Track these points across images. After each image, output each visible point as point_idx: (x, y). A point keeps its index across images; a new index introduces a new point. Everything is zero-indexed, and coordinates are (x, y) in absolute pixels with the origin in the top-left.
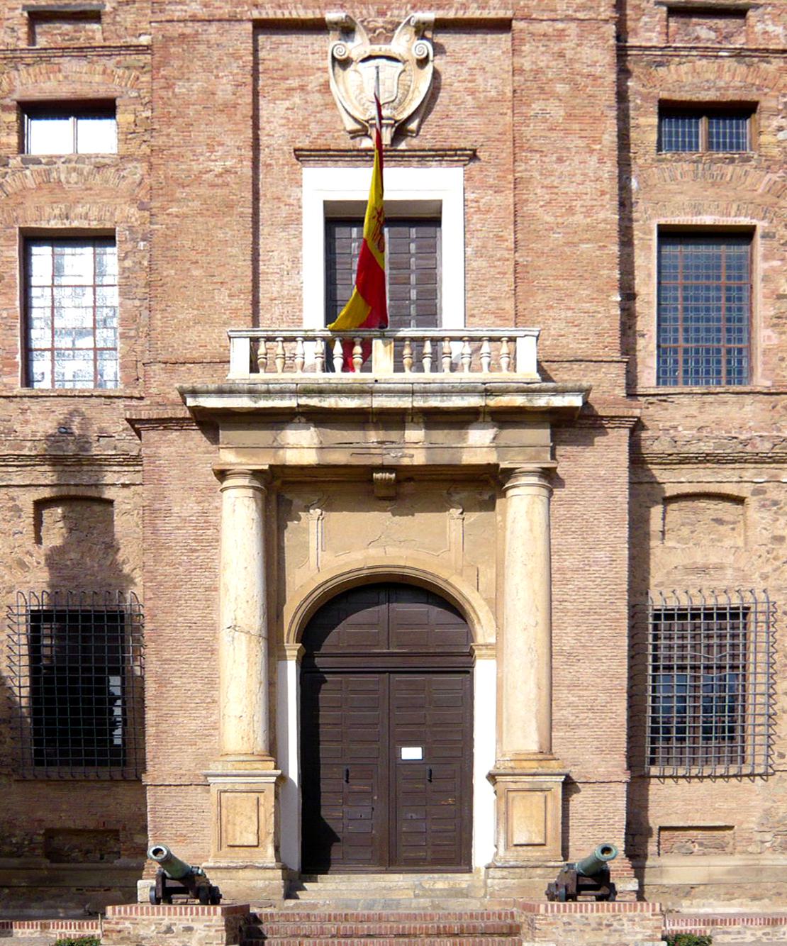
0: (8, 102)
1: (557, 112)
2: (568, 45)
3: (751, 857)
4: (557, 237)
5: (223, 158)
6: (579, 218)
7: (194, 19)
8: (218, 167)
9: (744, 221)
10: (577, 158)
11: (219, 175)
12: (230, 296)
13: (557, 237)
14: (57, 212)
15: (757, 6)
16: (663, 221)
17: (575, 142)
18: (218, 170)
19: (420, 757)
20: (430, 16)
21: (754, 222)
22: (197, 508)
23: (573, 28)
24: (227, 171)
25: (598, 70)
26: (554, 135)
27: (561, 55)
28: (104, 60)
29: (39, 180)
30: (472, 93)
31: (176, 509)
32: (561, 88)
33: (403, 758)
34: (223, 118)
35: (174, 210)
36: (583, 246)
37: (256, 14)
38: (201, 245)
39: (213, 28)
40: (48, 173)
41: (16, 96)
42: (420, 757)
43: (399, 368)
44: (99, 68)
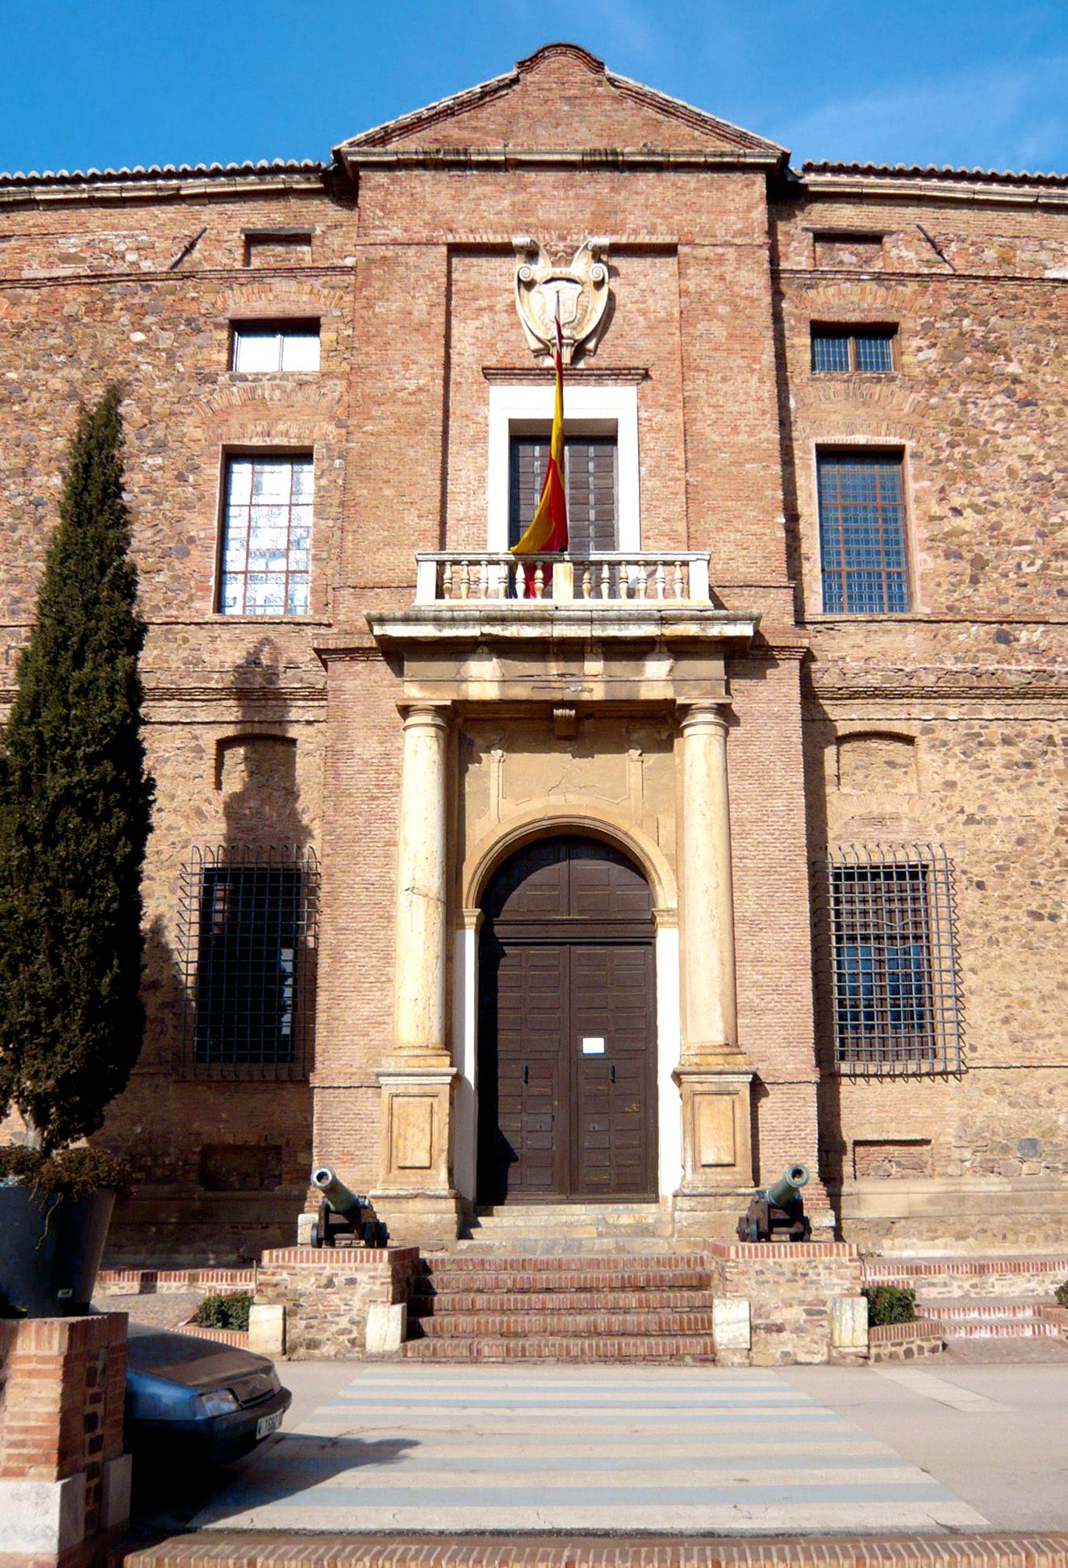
0: (221, 320)
1: (720, 332)
2: (728, 269)
6: (743, 438)
8: (412, 385)
9: (894, 440)
10: (739, 378)
11: (413, 393)
14: (259, 429)
15: (891, 233)
16: (820, 441)
18: (412, 388)
19: (602, 1050)
20: (605, 241)
21: (903, 441)
22: (380, 749)
23: (731, 253)
24: (420, 389)
26: (718, 355)
27: (722, 278)
28: (311, 281)
30: (644, 313)
31: (358, 751)
32: (722, 310)
35: (369, 428)
37: (450, 238)
38: (393, 464)
39: (412, 251)
41: (229, 315)
42: (602, 1050)
43: (578, 594)
44: (307, 288)
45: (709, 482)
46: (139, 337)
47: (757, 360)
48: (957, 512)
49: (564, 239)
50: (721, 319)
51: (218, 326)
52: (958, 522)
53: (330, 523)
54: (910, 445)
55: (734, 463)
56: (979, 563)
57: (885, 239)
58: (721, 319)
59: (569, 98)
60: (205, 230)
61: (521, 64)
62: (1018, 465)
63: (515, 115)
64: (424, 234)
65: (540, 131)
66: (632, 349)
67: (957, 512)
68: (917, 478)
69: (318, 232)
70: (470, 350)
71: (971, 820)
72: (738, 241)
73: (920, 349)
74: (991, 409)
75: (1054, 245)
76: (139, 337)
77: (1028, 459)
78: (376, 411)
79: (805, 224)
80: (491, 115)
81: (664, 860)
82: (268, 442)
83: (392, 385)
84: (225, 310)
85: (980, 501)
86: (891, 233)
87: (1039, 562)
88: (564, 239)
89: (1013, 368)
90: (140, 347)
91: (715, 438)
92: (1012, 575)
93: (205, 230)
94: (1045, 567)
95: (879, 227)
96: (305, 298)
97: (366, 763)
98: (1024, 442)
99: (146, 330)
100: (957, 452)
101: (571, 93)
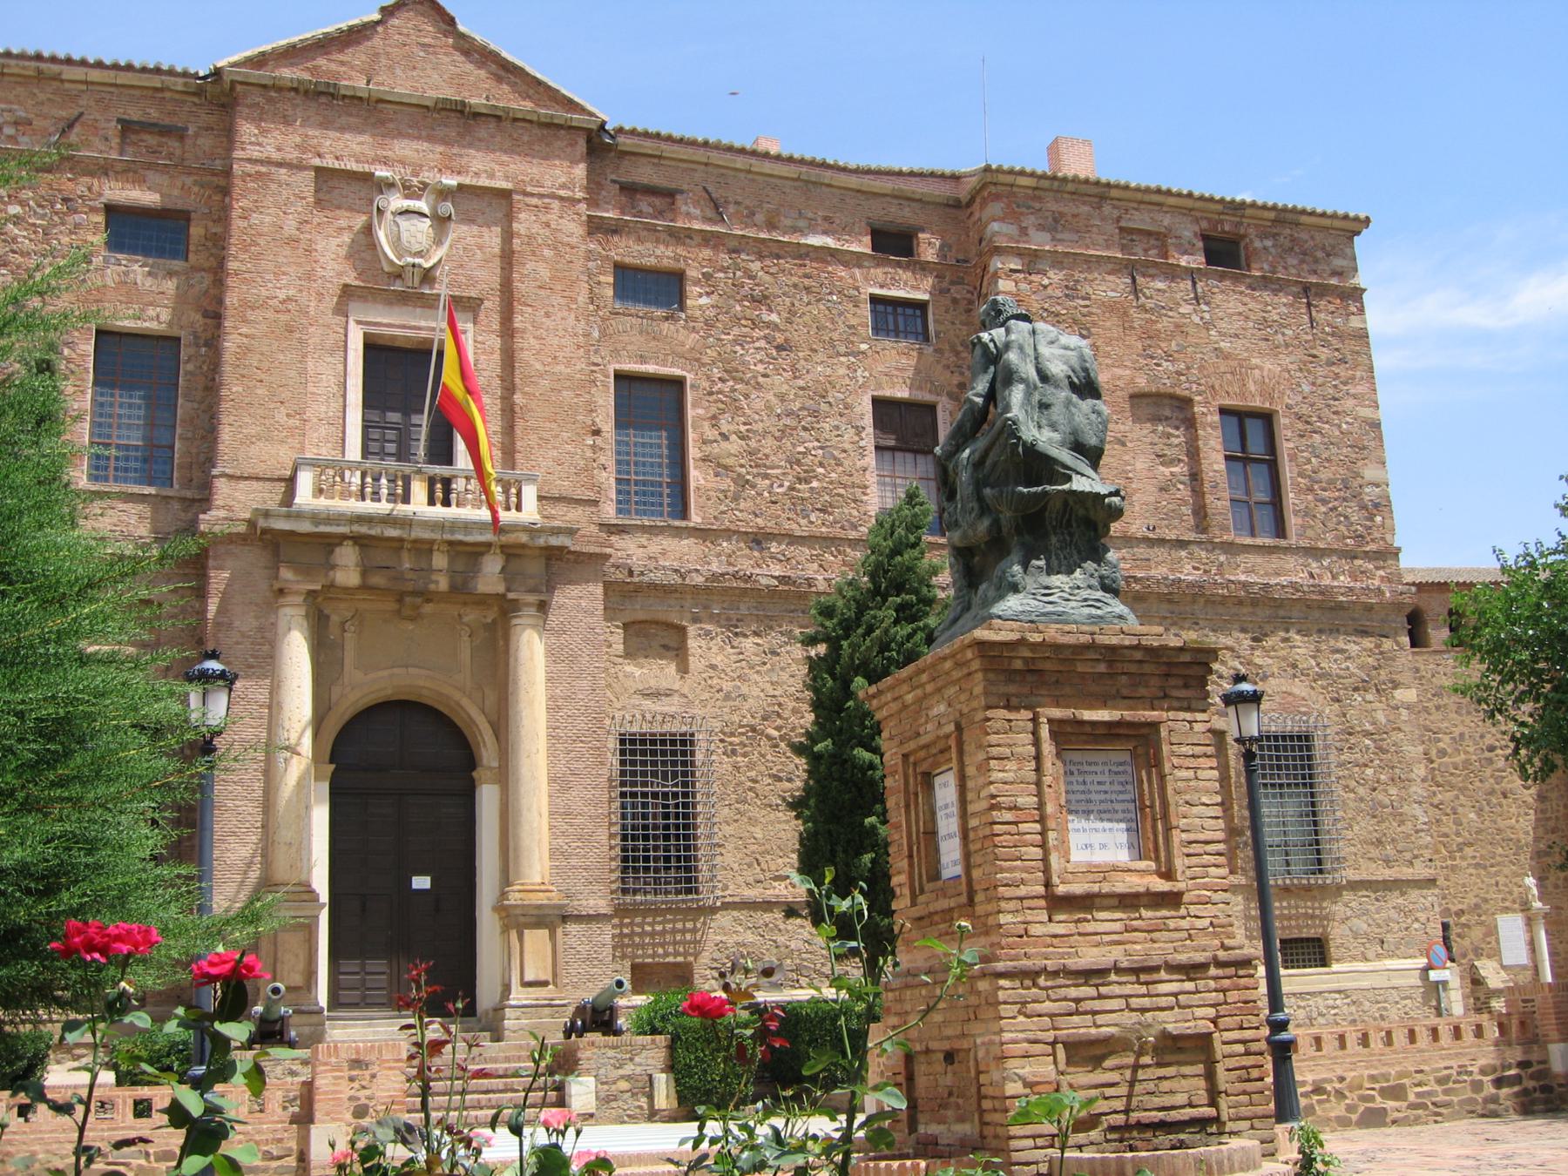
0: (97, 204)
1: (545, 273)
2: (552, 217)
3: (1335, 986)
4: (545, 383)
5: (287, 287)
6: (561, 368)
7: (268, 162)
8: (282, 295)
9: (677, 372)
10: (560, 315)
11: (283, 302)
12: (288, 415)
13: (545, 383)
14: (131, 312)
15: (682, 192)
16: (618, 367)
17: (557, 300)
18: (282, 296)
19: (414, 879)
20: (451, 181)
21: (684, 373)
22: (255, 624)
23: (556, 204)
24: (289, 299)
25: (573, 241)
26: (542, 292)
27: (548, 225)
28: (184, 178)
29: (117, 279)
30: (480, 248)
31: (237, 623)
32: (547, 253)
33: (414, 886)
34: (287, 251)
35: (244, 330)
36: (565, 393)
37: (317, 162)
38: (265, 365)
39: (283, 171)
40: (126, 274)
41: (103, 200)
42: (414, 879)
43: (431, 502)
44: (179, 184)
45: (533, 405)
46: (14, 209)
47: (574, 300)
48: (725, 437)
49: (417, 175)
50: (545, 260)
51: (93, 210)
52: (724, 445)
53: (196, 405)
54: (690, 377)
55: (553, 390)
56: (742, 483)
57: (678, 197)
58: (545, 260)
59: (424, 45)
60: (81, 114)
61: (383, 10)
62: (774, 400)
63: (377, 55)
64: (293, 155)
65: (398, 72)
66: (470, 278)
67: (725, 437)
68: (694, 406)
69: (190, 132)
70: (332, 265)
71: (727, 697)
72: (562, 193)
73: (700, 295)
74: (753, 358)
75: (810, 215)
76: (14, 209)
77: (782, 398)
78: (251, 315)
79: (614, 177)
80: (356, 56)
81: (487, 725)
82: (139, 324)
83: (264, 293)
84: (100, 195)
85: (743, 428)
86: (682, 192)
87: (787, 484)
88: (417, 175)
89: (774, 317)
90: (17, 220)
91: (538, 366)
92: (766, 494)
93: (81, 114)
94: (792, 488)
95: (673, 186)
96: (176, 192)
97: (243, 635)
98: (779, 382)
99: (23, 203)
100: (726, 387)
101: (426, 40)
